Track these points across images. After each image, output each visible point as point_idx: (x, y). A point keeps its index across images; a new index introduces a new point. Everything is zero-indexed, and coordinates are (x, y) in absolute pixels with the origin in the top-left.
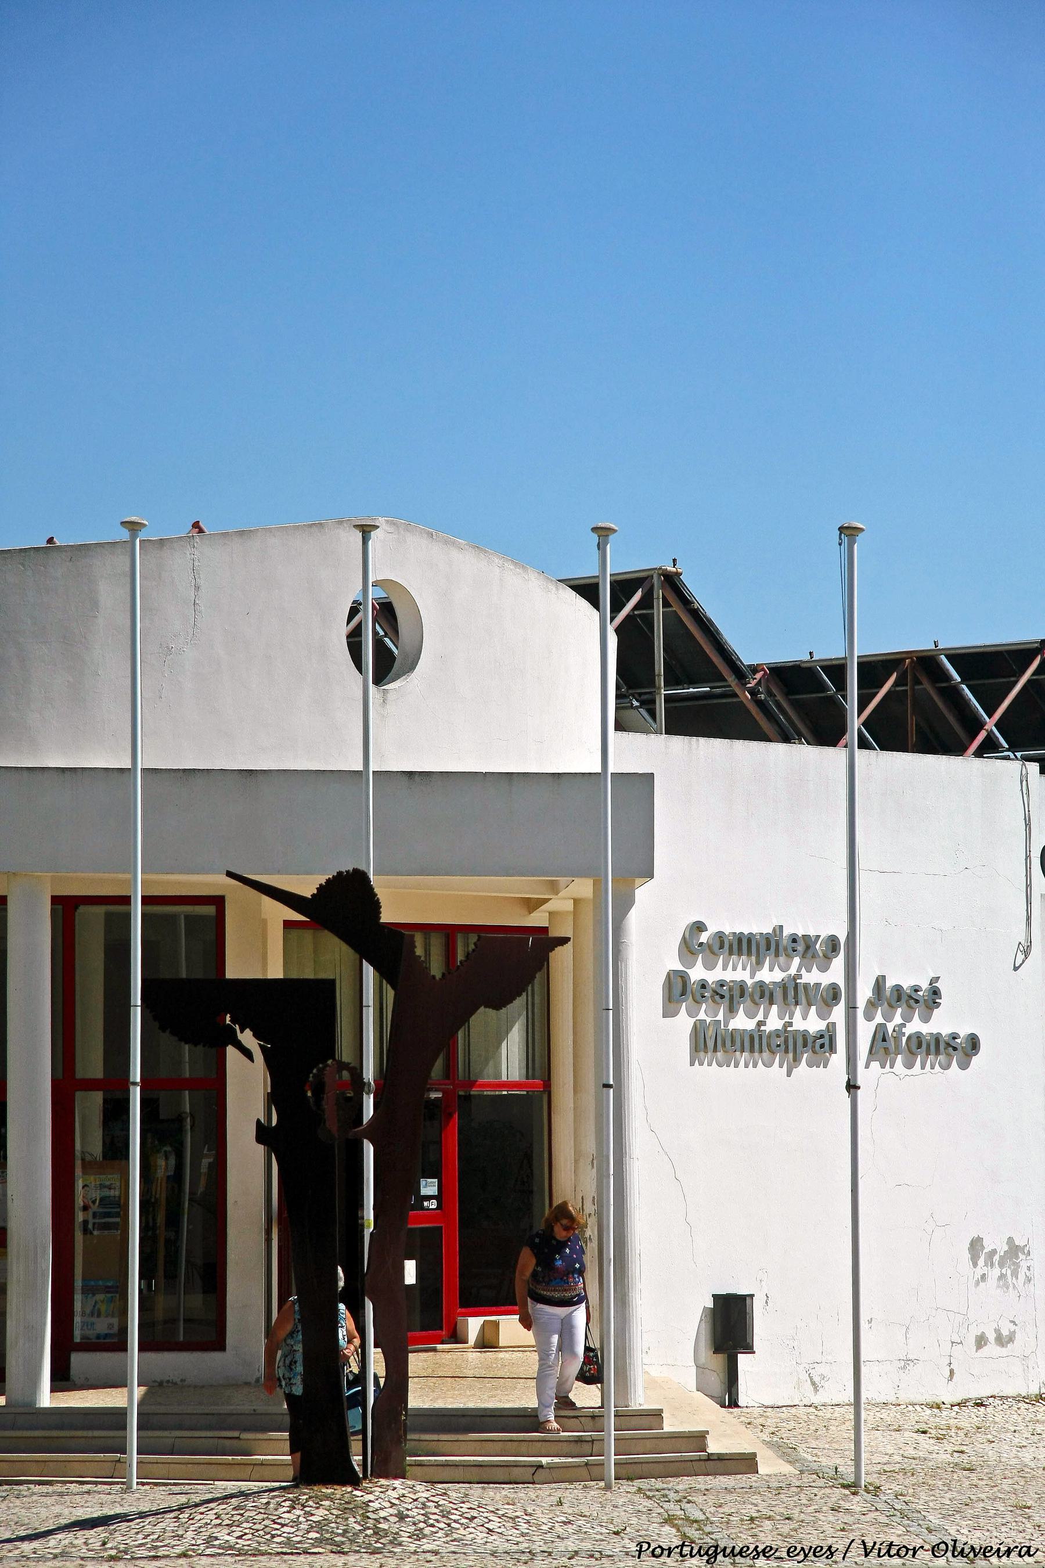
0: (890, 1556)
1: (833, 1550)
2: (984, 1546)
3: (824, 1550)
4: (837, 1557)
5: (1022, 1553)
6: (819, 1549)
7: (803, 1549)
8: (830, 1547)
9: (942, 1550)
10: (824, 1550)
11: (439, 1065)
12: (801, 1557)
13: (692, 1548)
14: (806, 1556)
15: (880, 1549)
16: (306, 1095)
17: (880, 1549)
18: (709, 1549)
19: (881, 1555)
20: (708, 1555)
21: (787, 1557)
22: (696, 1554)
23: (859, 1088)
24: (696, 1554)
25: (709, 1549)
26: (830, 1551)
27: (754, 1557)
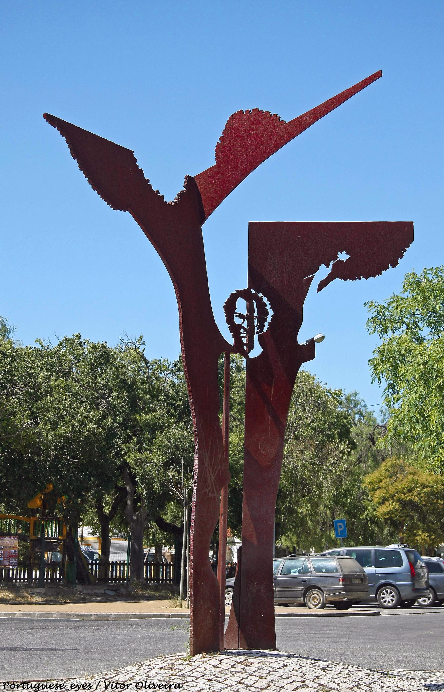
0: (146, 688)
1: (91, 685)
2: (83, 684)
3: (54, 686)
4: (93, 689)
5: (176, 687)
6: (52, 685)
7: (78, 685)
8: (90, 684)
9: (139, 686)
10: (54, 686)
11: (265, 330)
12: (77, 688)
13: (28, 685)
14: (79, 688)
15: (112, 685)
16: (217, 359)
17: (112, 685)
18: (35, 685)
19: (113, 687)
20: (35, 688)
21: (122, 690)
22: (147, 688)
23: (189, 179)
24: (147, 688)
25: (35, 685)
26: (90, 686)
27: (89, 688)
